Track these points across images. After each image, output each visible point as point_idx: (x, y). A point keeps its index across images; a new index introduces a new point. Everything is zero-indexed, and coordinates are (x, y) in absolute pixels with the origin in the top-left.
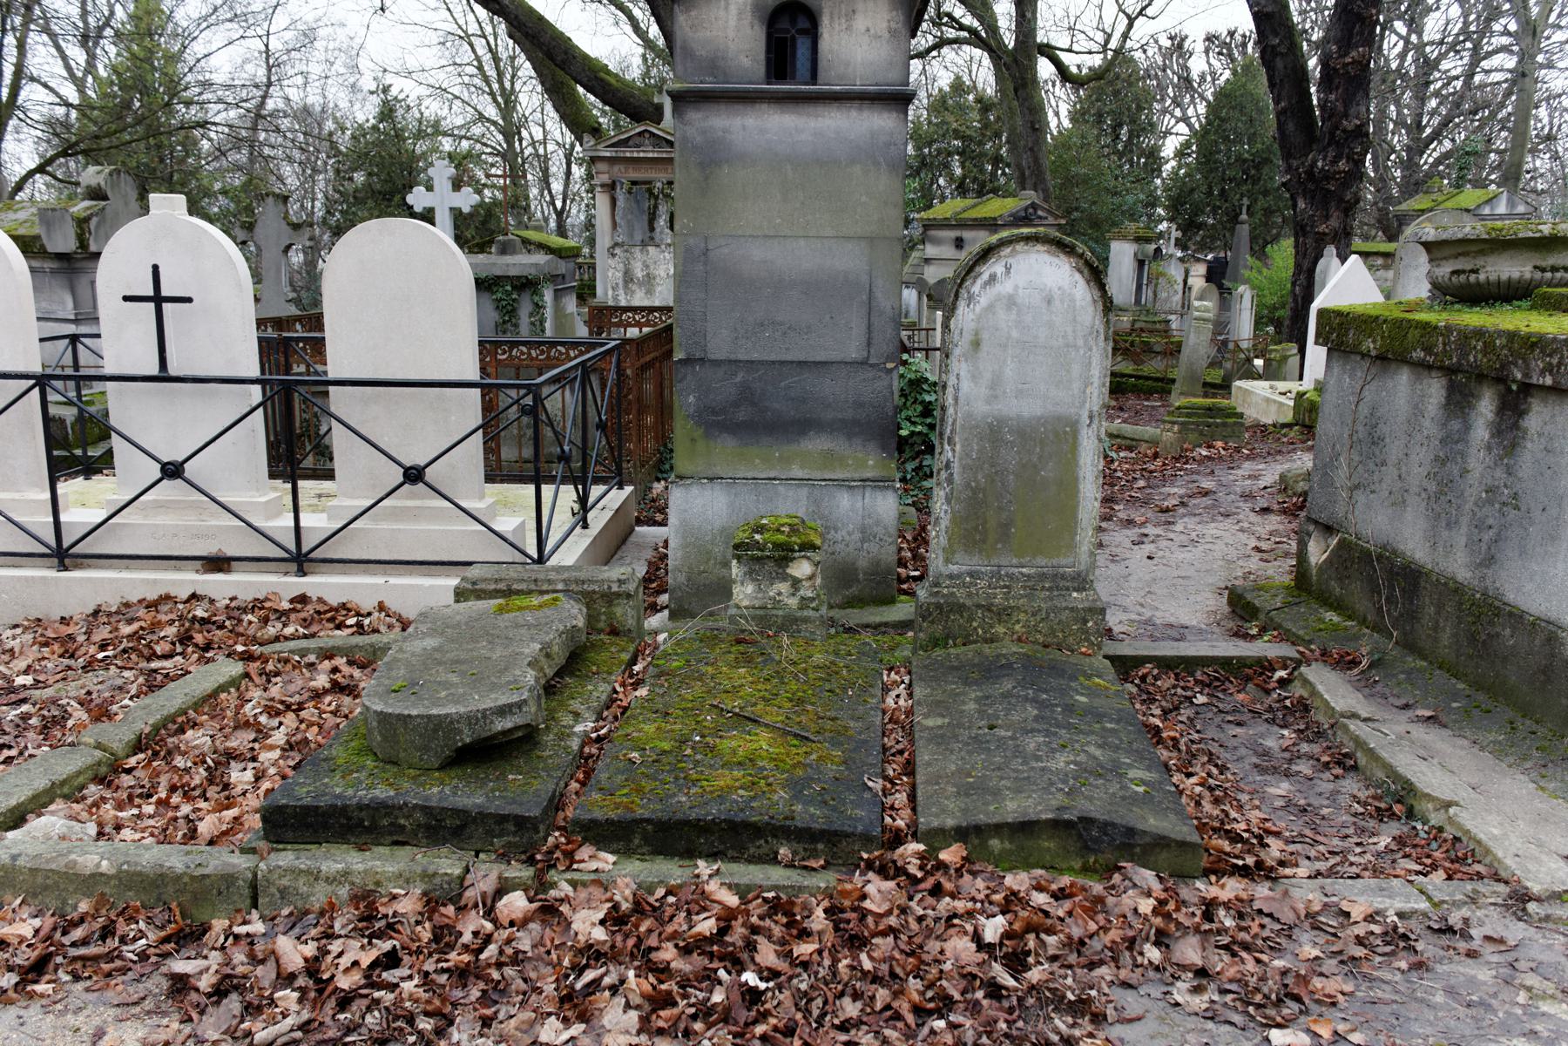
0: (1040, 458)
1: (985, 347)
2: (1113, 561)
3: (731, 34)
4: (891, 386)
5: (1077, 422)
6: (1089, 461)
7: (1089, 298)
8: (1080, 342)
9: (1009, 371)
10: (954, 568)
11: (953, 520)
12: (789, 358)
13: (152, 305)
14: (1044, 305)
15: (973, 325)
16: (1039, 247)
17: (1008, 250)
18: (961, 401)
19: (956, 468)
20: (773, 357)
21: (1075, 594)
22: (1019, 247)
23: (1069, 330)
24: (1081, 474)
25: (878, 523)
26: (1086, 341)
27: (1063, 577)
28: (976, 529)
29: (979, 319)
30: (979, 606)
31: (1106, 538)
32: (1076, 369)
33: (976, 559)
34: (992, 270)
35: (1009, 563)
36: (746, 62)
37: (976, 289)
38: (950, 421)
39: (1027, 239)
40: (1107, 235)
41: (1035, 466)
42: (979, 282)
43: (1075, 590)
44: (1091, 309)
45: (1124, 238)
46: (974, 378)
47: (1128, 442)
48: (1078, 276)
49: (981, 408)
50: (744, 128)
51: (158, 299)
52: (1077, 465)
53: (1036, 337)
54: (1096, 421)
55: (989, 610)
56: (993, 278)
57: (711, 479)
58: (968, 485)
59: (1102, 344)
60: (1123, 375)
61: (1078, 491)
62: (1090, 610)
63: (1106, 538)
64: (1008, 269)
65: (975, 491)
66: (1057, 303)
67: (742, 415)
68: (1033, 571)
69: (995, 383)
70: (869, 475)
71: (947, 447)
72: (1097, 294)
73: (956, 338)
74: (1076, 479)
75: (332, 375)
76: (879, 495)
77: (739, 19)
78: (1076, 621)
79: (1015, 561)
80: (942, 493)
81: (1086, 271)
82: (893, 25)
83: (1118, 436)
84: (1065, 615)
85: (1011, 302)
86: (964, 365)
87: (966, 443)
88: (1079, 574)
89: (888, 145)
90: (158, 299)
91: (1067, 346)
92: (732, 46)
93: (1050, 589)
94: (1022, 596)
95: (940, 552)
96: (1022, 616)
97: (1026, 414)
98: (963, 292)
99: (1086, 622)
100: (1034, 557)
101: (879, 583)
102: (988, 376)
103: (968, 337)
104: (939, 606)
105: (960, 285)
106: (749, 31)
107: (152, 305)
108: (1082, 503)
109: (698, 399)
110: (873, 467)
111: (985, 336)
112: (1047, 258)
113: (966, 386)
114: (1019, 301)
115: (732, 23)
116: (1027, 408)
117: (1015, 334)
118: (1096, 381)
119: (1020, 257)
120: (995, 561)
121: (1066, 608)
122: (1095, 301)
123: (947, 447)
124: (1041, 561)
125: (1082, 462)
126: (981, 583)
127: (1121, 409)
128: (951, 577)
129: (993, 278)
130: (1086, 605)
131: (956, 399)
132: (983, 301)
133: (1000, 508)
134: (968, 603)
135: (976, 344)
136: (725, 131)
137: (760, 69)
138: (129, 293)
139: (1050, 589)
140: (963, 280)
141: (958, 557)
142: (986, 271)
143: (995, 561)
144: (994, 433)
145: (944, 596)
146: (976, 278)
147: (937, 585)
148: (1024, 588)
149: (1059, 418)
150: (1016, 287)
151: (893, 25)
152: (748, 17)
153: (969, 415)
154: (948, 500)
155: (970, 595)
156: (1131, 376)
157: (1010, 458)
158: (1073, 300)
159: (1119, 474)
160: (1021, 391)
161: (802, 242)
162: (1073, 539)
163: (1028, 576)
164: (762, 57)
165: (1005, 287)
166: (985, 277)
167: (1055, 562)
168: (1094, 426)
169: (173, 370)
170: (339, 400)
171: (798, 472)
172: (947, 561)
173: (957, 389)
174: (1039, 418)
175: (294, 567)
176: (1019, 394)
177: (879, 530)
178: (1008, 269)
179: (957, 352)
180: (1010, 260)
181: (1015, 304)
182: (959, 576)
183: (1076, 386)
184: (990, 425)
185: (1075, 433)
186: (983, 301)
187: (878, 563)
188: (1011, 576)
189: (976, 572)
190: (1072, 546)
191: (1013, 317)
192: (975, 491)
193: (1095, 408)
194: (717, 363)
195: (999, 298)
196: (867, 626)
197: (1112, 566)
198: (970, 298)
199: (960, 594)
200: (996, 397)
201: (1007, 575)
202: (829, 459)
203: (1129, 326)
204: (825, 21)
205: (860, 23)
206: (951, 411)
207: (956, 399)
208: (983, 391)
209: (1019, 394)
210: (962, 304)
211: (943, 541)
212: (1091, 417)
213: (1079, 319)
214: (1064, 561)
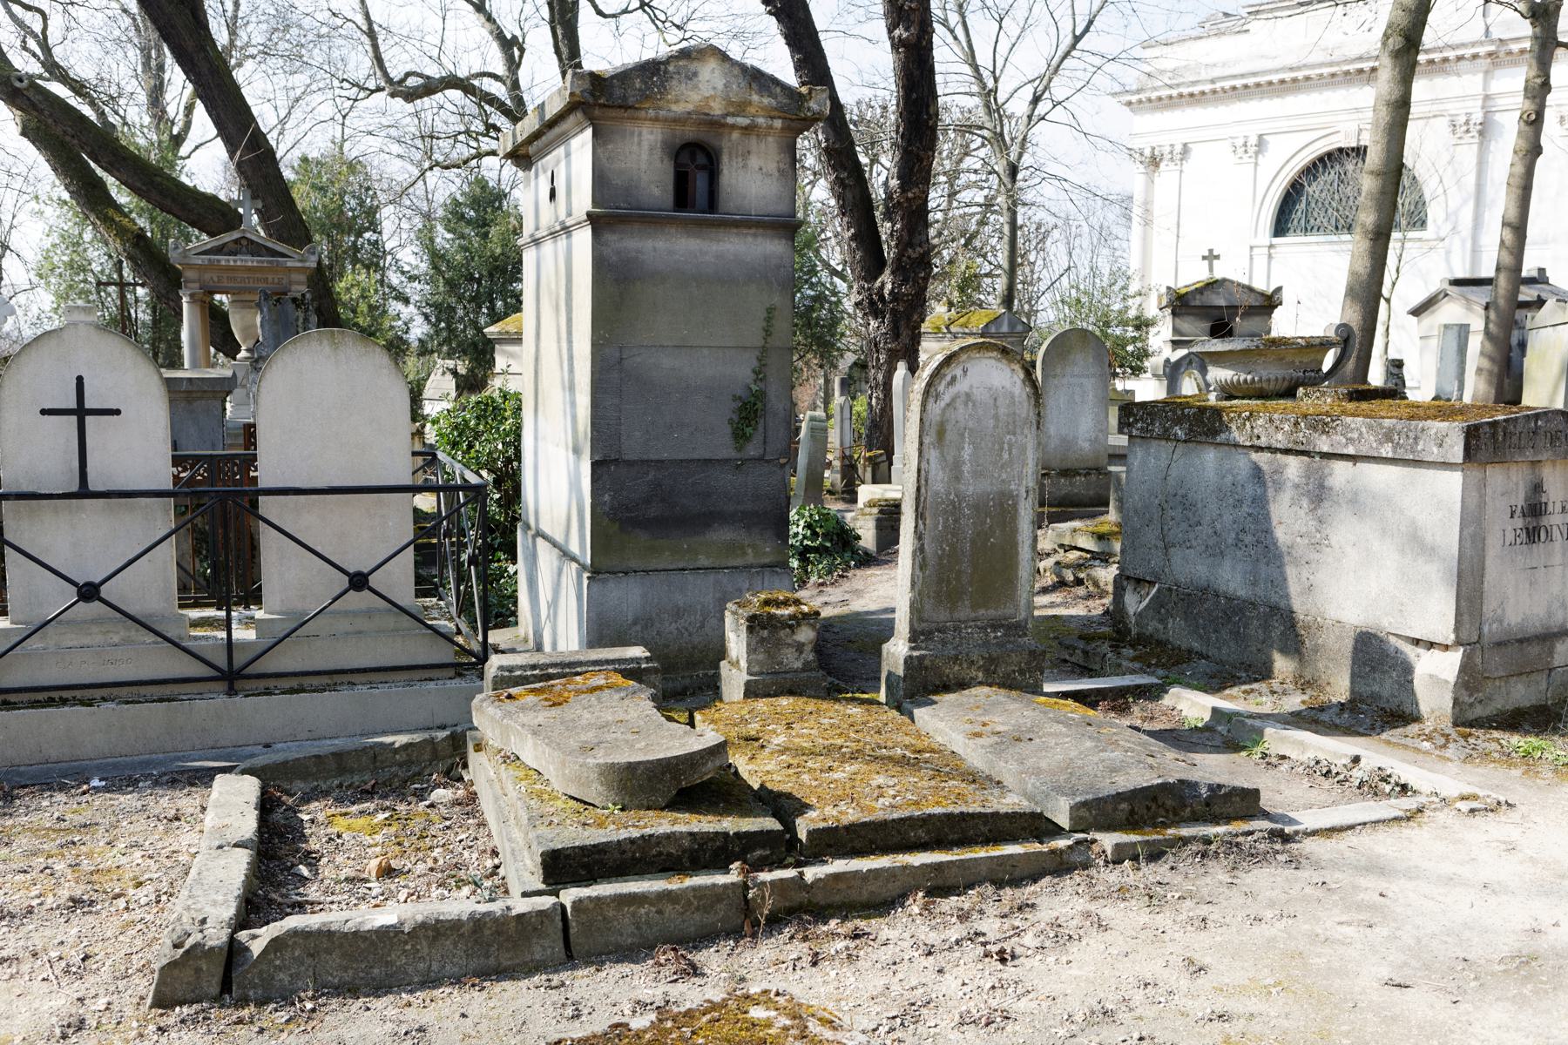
3: (644, 166)
12: (695, 456)
13: (74, 418)
20: (681, 456)
29: (944, 410)
36: (656, 192)
42: (944, 383)
50: (655, 249)
51: (81, 412)
57: (647, 572)
64: (965, 372)
67: (654, 511)
70: (767, 561)
75: (262, 484)
77: (651, 154)
82: (782, 166)
89: (778, 267)
90: (81, 412)
92: (645, 178)
106: (658, 165)
107: (74, 418)
109: (613, 498)
115: (644, 157)
129: (954, 379)
132: (947, 398)
136: (638, 251)
137: (669, 199)
138: (47, 406)
142: (949, 373)
151: (782, 166)
152: (658, 153)
161: (706, 351)
164: (671, 187)
165: (962, 386)
166: (948, 378)
169: (95, 484)
170: (267, 506)
171: (703, 561)
175: (222, 686)
194: (630, 464)
202: (733, 548)
204: (725, 159)
205: (754, 162)
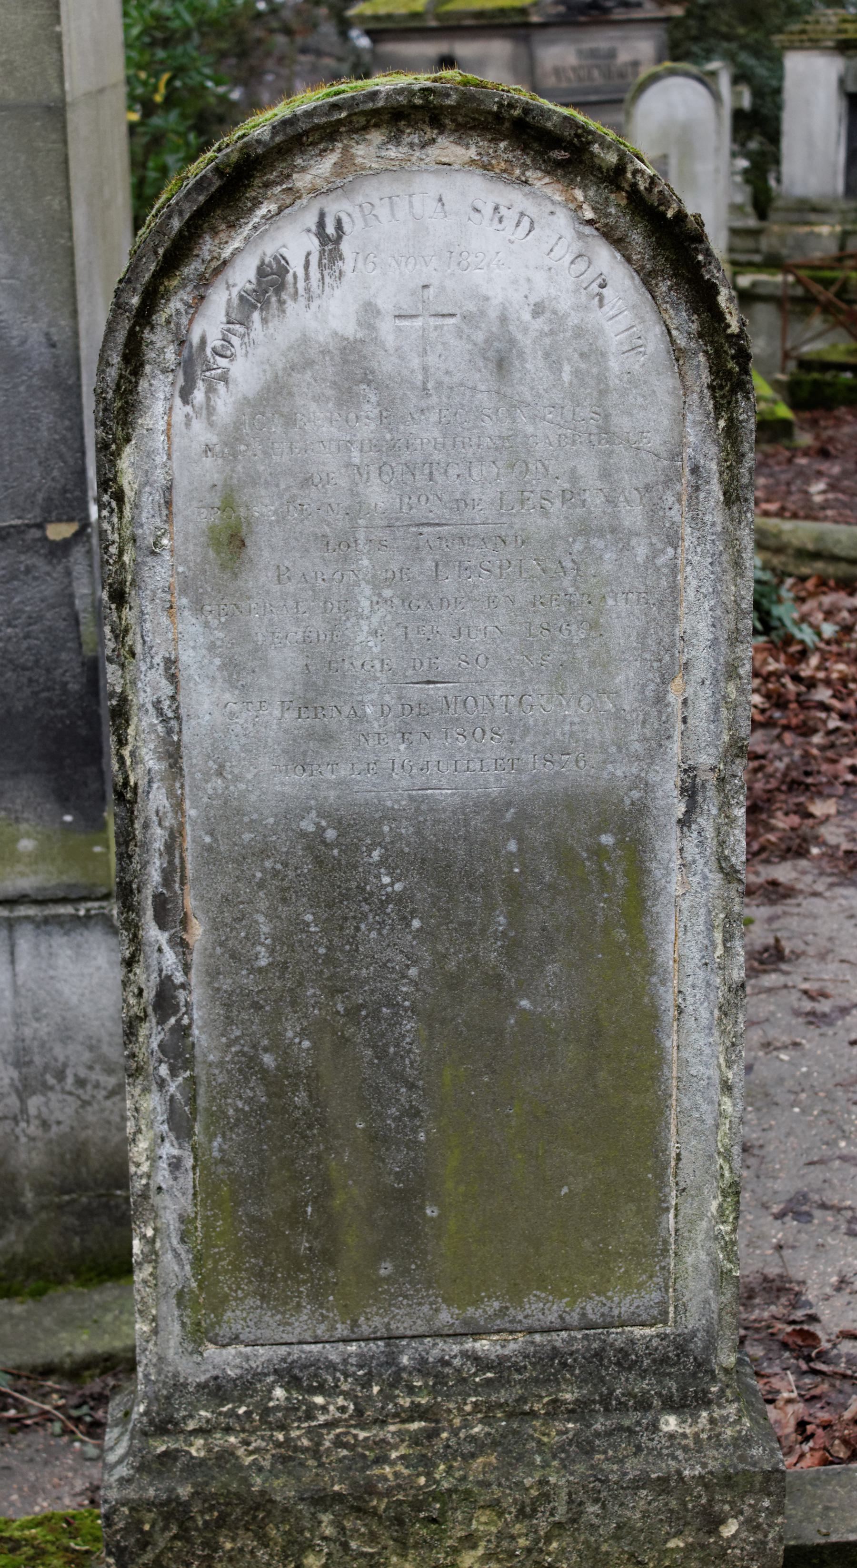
0: (512, 948)
1: (265, 552)
2: (814, 1018)
4: (69, 598)
5: (640, 810)
6: (693, 953)
7: (654, 340)
8: (633, 515)
9: (370, 635)
10: (225, 1360)
11: (207, 1192)
14: (483, 379)
15: (210, 469)
16: (447, 148)
17: (324, 166)
18: (193, 759)
19: (198, 1005)
21: (670, 1423)
22: (369, 149)
23: (588, 468)
24: (668, 999)
25: (65, 1034)
26: (654, 512)
27: (625, 1359)
28: (293, 1215)
29: (232, 441)
30: (322, 1500)
31: (794, 925)
32: (623, 616)
33: (302, 1323)
34: (269, 248)
35: (432, 1327)
37: (210, 325)
38: (158, 837)
39: (406, 117)
40: (777, 39)
41: (496, 981)
42: (220, 299)
43: (672, 1405)
44: (664, 385)
45: (813, 44)
46: (236, 670)
47: (843, 569)
48: (605, 257)
49: (271, 783)
52: (650, 966)
53: (462, 502)
54: (710, 805)
55: (360, 1511)
56: (273, 280)
58: (249, 1064)
59: (714, 513)
60: (825, 366)
61: (660, 1061)
62: (728, 1480)
63: (794, 925)
64: (330, 241)
65: (275, 1085)
66: (533, 365)
68: (515, 1345)
69: (319, 689)
71: (153, 933)
72: (685, 323)
73: (149, 521)
74: (652, 1017)
76: (61, 946)
78: (678, 1521)
79: (445, 1317)
80: (153, 1102)
81: (637, 238)
83: (816, 555)
84: (637, 1508)
85: (352, 369)
86: (190, 626)
87: (229, 915)
88: (682, 1345)
91: (584, 529)
93: (580, 1411)
94: (480, 1446)
95: (169, 1310)
96: (483, 1522)
97: (444, 794)
98: (160, 345)
99: (714, 1522)
100: (516, 1295)
101: (86, 1214)
102: (286, 660)
103: (194, 517)
104: (173, 1511)
105: (144, 316)
108: (678, 1102)
110: (38, 858)
111: (263, 507)
112: (479, 189)
113: (206, 704)
114: (385, 365)
116: (447, 772)
117: (378, 495)
118: (702, 658)
119: (373, 192)
120: (373, 1321)
121: (641, 1482)
122: (678, 354)
123: (153, 933)
124: (542, 1308)
125: (666, 955)
126: (330, 1407)
127: (824, 454)
128: (217, 1390)
129: (273, 280)
130: (714, 1460)
131: (173, 754)
132: (245, 372)
133: (378, 1138)
134: (283, 1489)
135: (232, 542)
139: (580, 1411)
140: (153, 297)
141: (235, 1318)
142: (244, 252)
143: (373, 1321)
144: (329, 869)
145: (194, 1467)
146: (204, 282)
147: (163, 1425)
148: (487, 1412)
149: (572, 803)
150: (369, 312)
153: (228, 813)
154: (180, 1124)
155: (288, 1458)
156: (842, 367)
157: (400, 958)
158: (594, 354)
159: (823, 694)
160: (421, 710)
162: (652, 1226)
163: (500, 1365)
165: (325, 314)
166: (243, 275)
167: (593, 1309)
168: (705, 822)
172: (198, 1335)
173: (172, 718)
174: (497, 807)
176: (414, 721)
177: (75, 1056)
178: (330, 241)
179: (158, 575)
180: (335, 207)
181: (368, 378)
182: (246, 1385)
183: (627, 676)
184: (314, 843)
185: (636, 850)
186: (245, 372)
187: (80, 1153)
188: (436, 1373)
189: (313, 1365)
190: (651, 1252)
191: (367, 430)
192: (275, 1085)
193: (705, 759)
195: (302, 357)
196: (48, 1371)
197: (810, 1038)
198: (191, 366)
199: (250, 1451)
200: (327, 738)
201: (422, 1367)
203: (833, 249)
206: (157, 799)
207: (173, 754)
208: (276, 718)
209: (413, 721)
210: (158, 392)
211: (176, 1268)
212: (690, 792)
213: (622, 423)
214: (624, 1306)
